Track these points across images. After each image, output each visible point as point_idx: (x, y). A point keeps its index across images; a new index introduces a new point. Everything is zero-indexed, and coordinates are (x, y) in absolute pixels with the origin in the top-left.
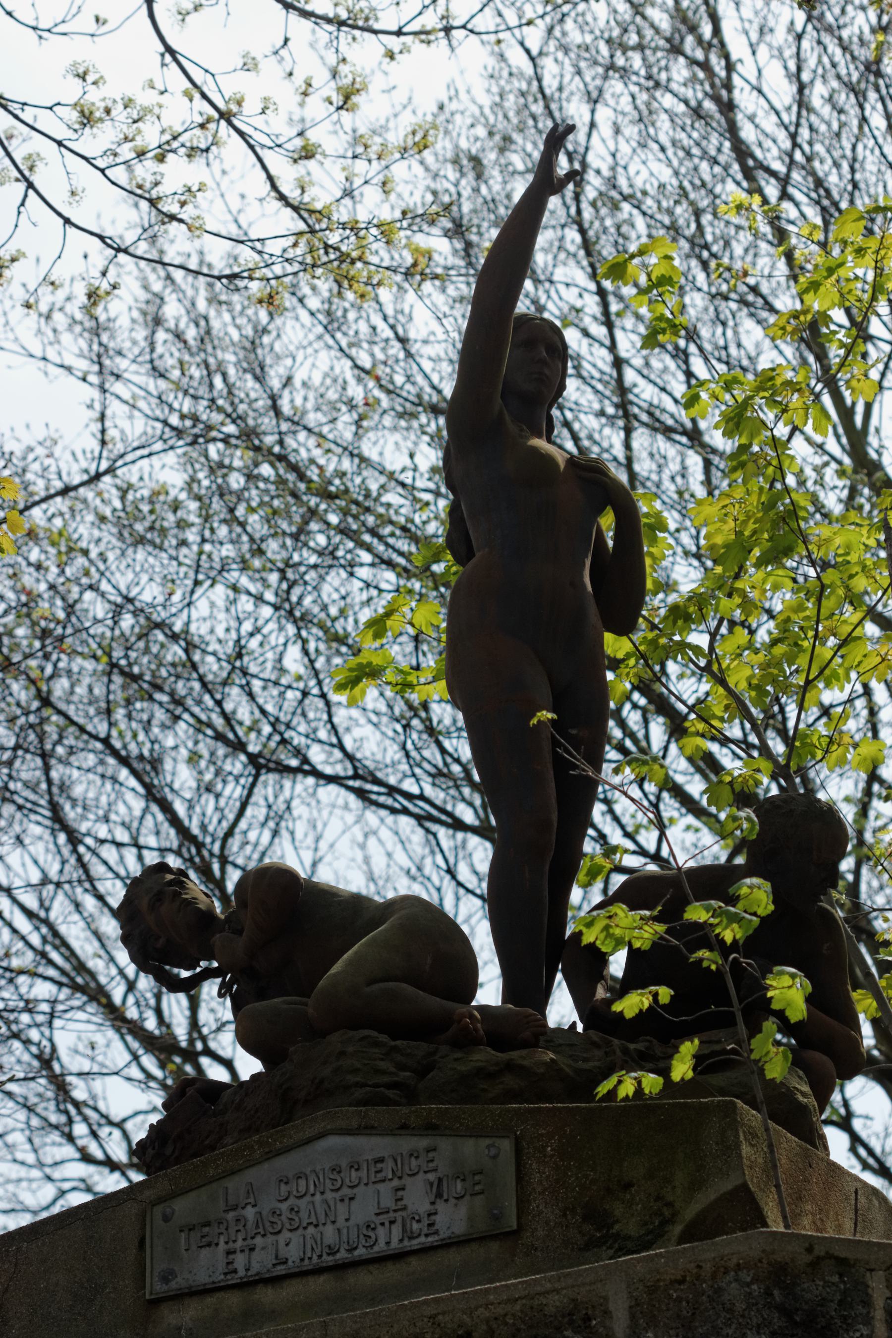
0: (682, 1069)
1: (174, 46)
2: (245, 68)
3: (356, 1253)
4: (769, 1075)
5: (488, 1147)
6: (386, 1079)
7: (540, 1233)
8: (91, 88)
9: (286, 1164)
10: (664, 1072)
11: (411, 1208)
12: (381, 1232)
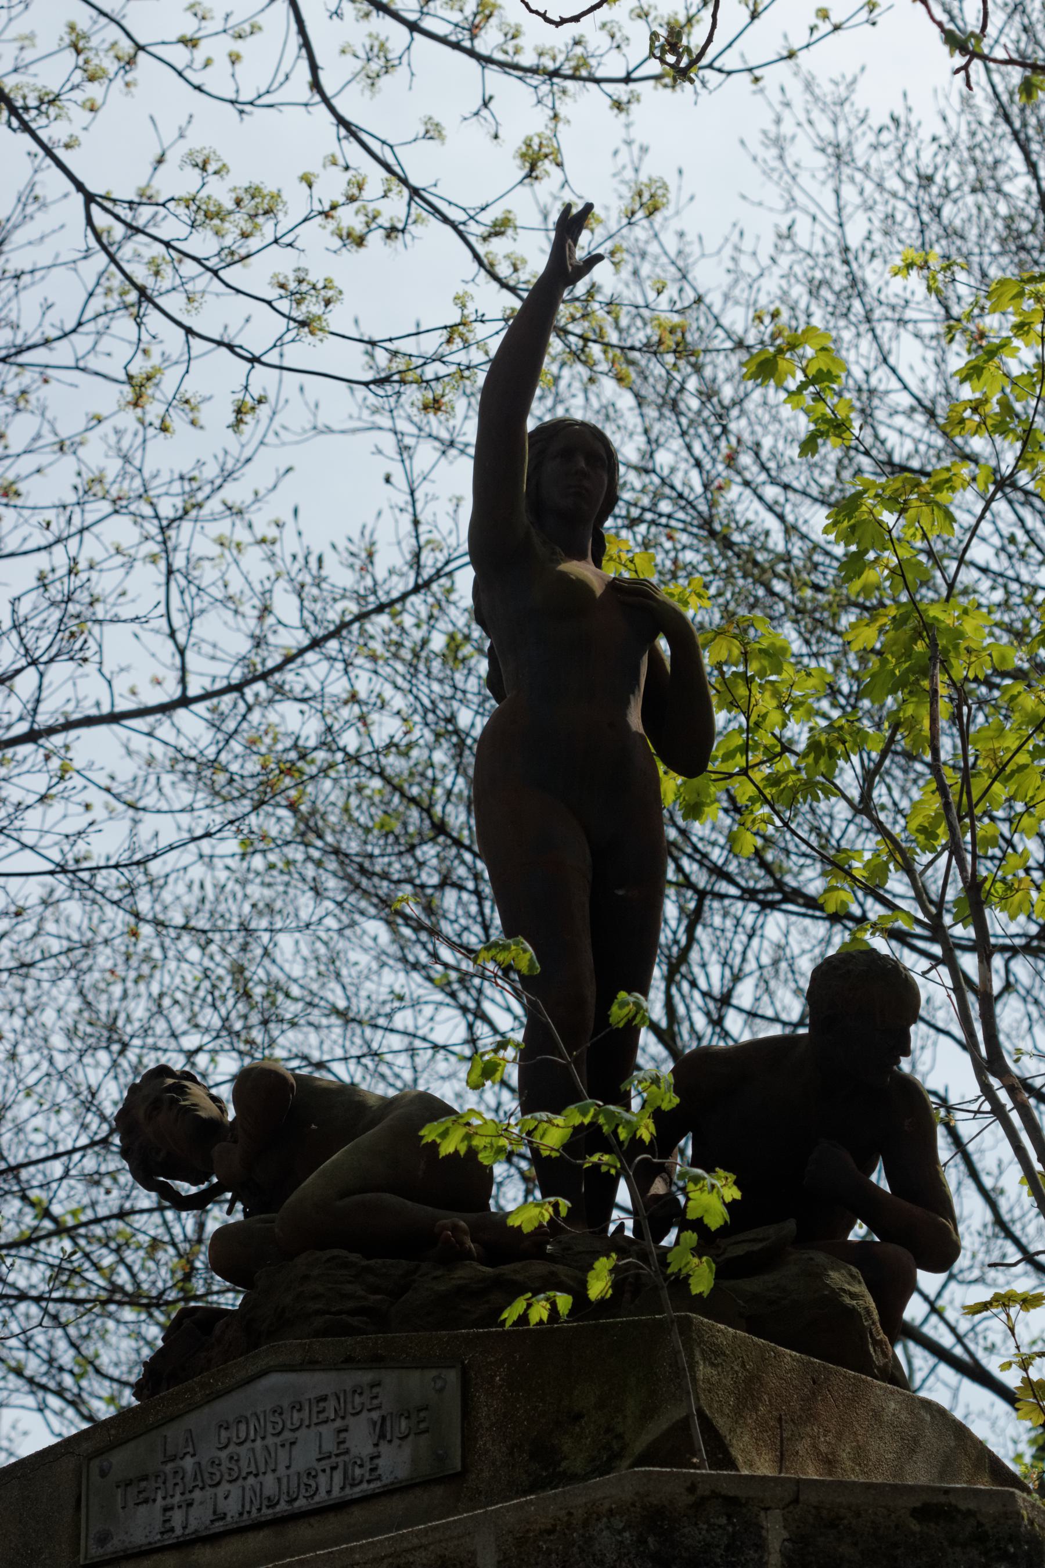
0: (598, 1286)
1: (349, 117)
2: (427, 136)
3: (297, 1504)
4: (695, 1290)
5: (434, 1379)
7: (486, 1474)
8: (213, 179)
9: (226, 1407)
10: (579, 1292)
11: (354, 1451)
12: (323, 1479)
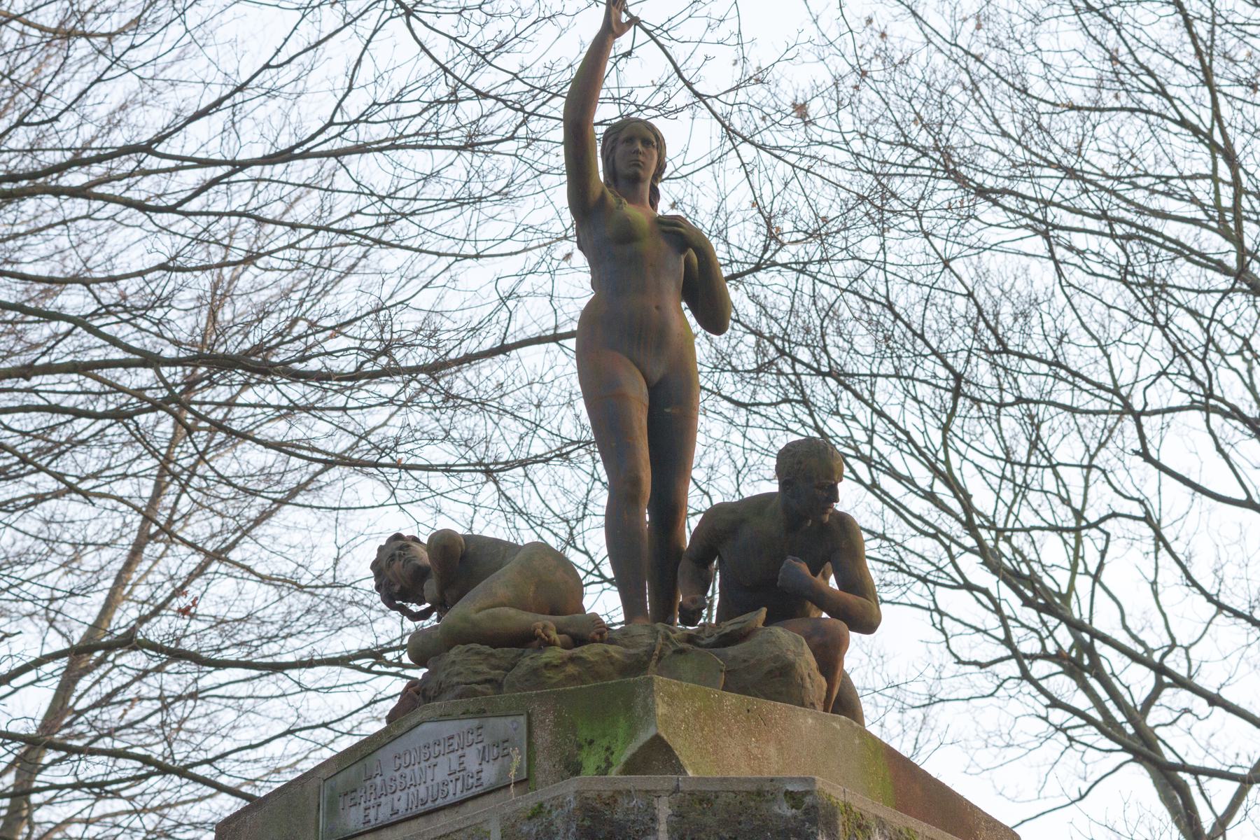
6: (479, 678)
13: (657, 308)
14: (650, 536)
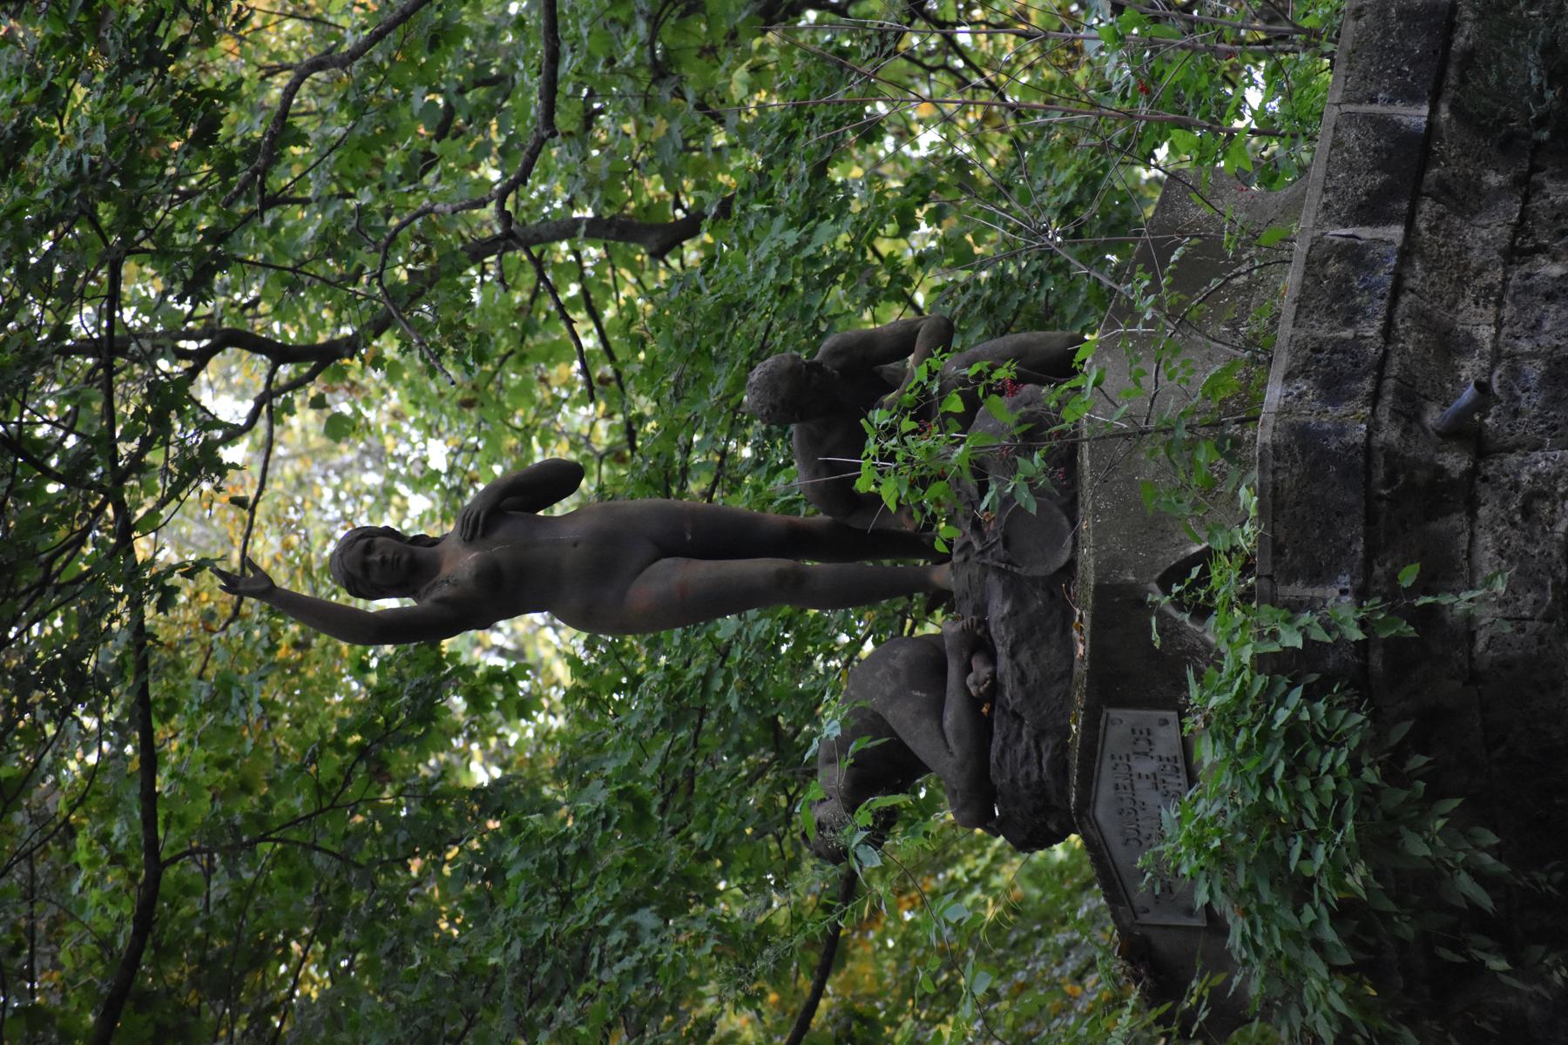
13: (575, 545)
14: (828, 561)
